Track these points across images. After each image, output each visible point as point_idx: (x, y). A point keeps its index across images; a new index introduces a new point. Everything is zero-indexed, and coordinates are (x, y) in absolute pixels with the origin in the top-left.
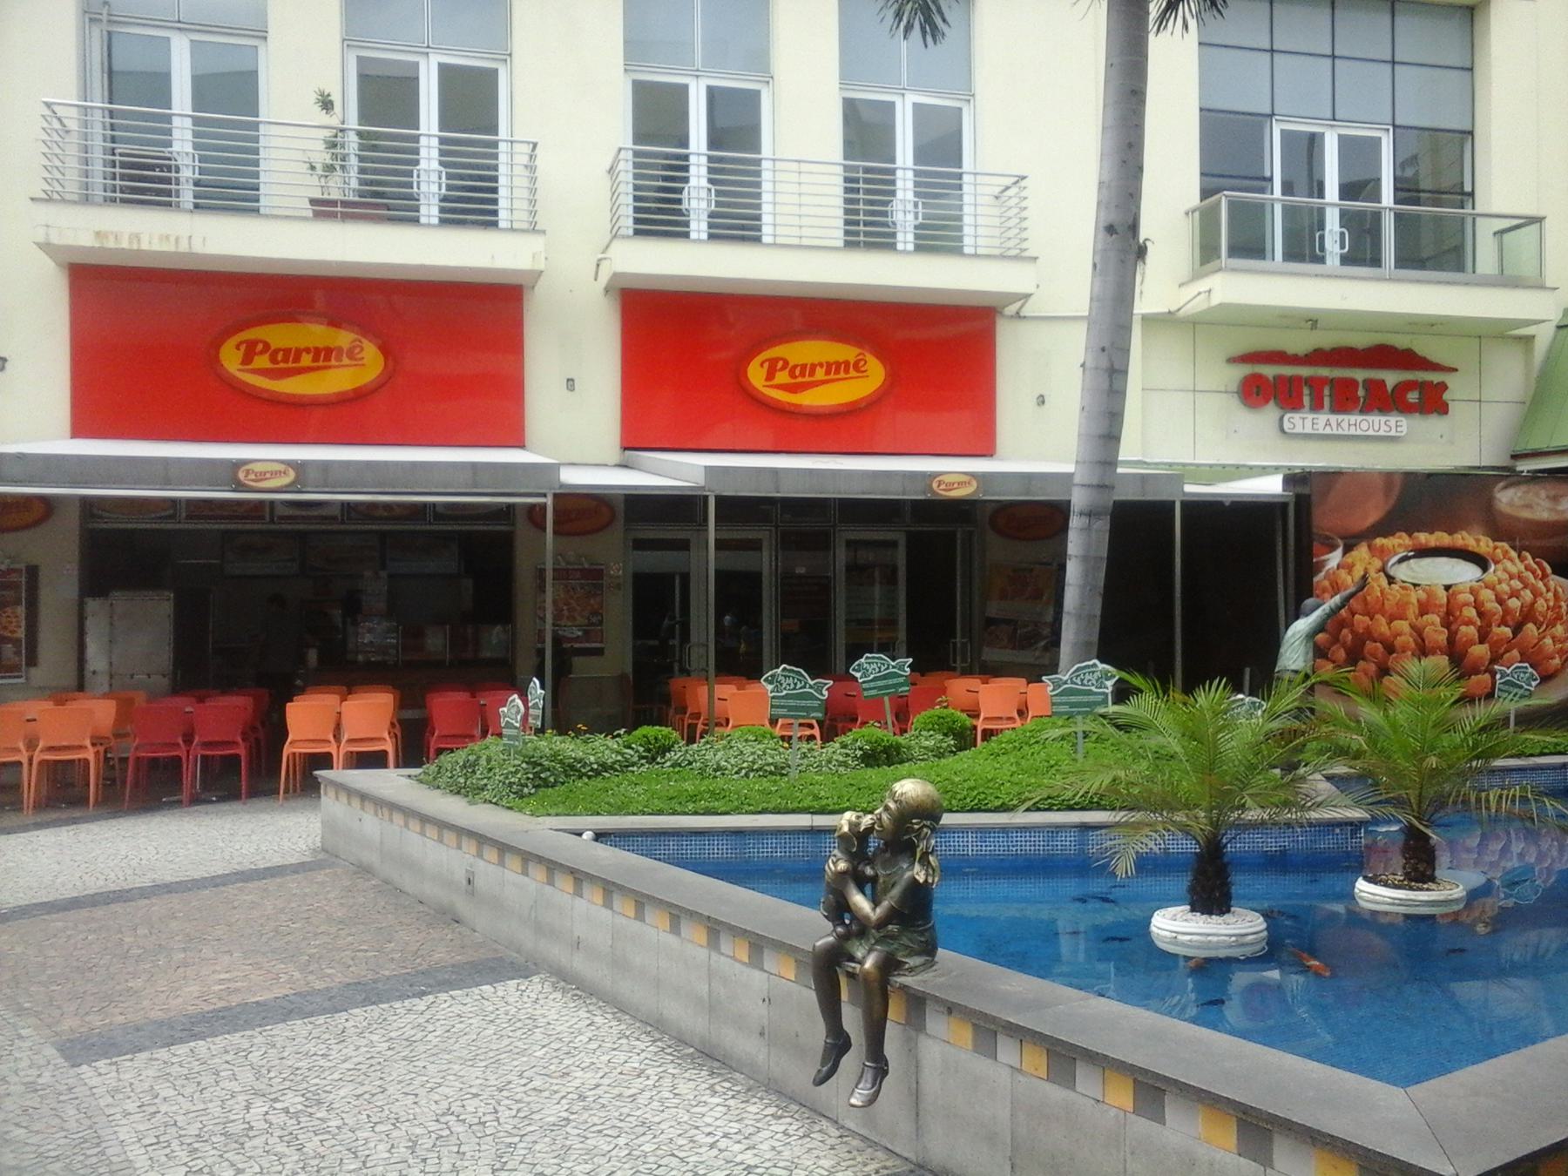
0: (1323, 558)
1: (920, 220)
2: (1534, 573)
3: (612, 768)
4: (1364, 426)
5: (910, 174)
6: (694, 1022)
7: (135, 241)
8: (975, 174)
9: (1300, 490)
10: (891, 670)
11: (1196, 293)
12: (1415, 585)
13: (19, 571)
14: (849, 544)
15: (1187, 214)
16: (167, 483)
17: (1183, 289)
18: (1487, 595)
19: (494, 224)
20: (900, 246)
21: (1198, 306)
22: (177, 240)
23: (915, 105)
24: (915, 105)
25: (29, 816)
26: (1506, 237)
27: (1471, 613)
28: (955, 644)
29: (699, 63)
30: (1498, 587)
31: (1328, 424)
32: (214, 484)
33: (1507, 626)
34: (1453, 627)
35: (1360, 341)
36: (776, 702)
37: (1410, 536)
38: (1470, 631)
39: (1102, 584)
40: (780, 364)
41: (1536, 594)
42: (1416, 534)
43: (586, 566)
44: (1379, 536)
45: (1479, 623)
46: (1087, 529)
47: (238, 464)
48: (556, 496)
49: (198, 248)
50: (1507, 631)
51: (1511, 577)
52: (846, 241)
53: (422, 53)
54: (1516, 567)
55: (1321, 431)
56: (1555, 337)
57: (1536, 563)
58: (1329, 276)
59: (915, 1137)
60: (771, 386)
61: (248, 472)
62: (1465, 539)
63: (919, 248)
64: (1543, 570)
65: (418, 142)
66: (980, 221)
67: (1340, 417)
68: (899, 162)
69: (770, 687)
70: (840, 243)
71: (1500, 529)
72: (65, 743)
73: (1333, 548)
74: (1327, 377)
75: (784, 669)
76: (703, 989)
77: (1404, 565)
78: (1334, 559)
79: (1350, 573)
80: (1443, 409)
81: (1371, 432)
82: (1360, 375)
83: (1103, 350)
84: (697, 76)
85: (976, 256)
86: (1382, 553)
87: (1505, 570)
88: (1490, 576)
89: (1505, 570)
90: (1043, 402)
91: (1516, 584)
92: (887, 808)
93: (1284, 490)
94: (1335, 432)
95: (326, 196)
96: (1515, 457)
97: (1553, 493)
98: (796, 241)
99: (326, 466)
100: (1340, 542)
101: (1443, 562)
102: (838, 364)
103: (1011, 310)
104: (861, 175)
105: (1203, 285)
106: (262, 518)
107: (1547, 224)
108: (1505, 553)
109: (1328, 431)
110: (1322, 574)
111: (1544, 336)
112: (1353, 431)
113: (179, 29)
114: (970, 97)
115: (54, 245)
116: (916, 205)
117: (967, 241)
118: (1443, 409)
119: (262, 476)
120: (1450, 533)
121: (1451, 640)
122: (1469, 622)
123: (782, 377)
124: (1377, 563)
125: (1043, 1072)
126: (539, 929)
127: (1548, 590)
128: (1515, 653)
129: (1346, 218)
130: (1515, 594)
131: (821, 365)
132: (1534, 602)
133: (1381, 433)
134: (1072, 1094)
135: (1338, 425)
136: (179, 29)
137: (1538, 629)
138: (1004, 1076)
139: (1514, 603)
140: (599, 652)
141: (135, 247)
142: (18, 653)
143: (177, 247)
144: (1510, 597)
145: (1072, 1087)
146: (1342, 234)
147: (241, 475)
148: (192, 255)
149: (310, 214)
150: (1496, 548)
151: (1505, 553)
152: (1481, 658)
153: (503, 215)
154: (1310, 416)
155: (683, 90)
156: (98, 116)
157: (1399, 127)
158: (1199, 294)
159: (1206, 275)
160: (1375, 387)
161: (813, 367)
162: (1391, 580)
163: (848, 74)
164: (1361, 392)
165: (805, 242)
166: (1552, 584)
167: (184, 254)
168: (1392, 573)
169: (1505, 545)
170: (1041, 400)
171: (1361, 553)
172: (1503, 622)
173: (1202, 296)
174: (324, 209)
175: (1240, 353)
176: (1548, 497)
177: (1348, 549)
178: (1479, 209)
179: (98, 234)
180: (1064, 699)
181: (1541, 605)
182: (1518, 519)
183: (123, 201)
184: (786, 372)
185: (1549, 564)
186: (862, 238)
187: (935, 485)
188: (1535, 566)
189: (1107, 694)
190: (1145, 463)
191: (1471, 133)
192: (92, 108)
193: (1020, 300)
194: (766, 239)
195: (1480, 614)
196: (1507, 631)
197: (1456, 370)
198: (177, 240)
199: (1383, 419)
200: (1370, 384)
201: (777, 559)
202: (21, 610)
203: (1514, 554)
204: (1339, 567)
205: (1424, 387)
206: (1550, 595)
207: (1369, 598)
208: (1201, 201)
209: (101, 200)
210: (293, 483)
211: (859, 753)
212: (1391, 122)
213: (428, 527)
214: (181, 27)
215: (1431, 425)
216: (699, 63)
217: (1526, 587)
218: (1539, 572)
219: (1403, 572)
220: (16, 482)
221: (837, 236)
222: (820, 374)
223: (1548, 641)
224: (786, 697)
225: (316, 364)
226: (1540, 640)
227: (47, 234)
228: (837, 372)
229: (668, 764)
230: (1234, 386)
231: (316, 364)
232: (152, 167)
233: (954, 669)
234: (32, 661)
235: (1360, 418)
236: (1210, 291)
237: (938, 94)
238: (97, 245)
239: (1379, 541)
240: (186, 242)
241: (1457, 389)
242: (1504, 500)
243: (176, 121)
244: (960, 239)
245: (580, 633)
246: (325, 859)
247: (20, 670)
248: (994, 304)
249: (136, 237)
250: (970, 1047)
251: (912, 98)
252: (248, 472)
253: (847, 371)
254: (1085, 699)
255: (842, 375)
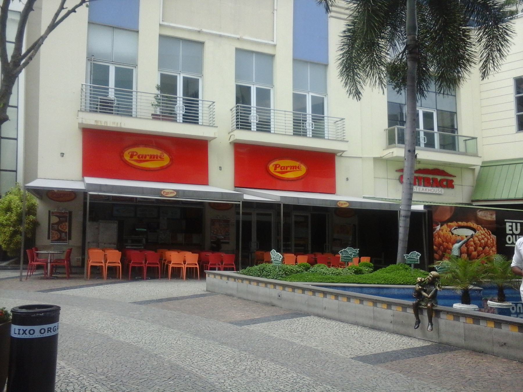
0: (436, 227)
1: (313, 128)
2: (487, 233)
3: (299, 272)
4: (433, 190)
5: (311, 116)
6: (371, 322)
7: (106, 123)
8: (328, 117)
9: (429, 209)
10: (354, 252)
11: (389, 152)
12: (458, 235)
13: (67, 213)
14: (295, 216)
15: (385, 130)
16: (143, 194)
17: (384, 151)
18: (476, 239)
19: (198, 123)
20: (308, 136)
21: (390, 156)
22: (117, 124)
23: (312, 96)
24: (312, 96)
25: (105, 281)
26: (468, 142)
27: (472, 243)
28: (326, 245)
29: (254, 81)
30: (479, 237)
31: (423, 189)
32: (155, 195)
33: (481, 247)
34: (468, 247)
35: (430, 167)
36: (342, 258)
37: (457, 222)
38: (472, 248)
39: (408, 233)
40: (278, 166)
41: (488, 239)
42: (458, 222)
43: (225, 219)
44: (449, 222)
45: (474, 246)
46: (405, 221)
47: (161, 190)
48: (242, 202)
49: (123, 126)
50: (481, 248)
51: (482, 234)
52: (294, 133)
53: (178, 73)
54: (483, 232)
55: (421, 192)
56: (480, 169)
57: (488, 231)
58: (421, 150)
59: (438, 337)
60: (276, 172)
61: (164, 192)
62: (470, 224)
63: (313, 137)
64: (489, 233)
65: (177, 99)
66: (329, 130)
67: (426, 188)
68: (308, 112)
69: (341, 254)
70: (292, 134)
71: (479, 222)
72: (114, 261)
73: (438, 225)
74: (422, 177)
75: (344, 250)
76: (372, 315)
77: (455, 230)
78: (438, 228)
79: (442, 232)
80: (452, 187)
81: (434, 192)
82: (431, 176)
83: (408, 179)
84: (253, 84)
85: (328, 139)
86: (450, 227)
87: (480, 232)
88: (477, 234)
89: (480, 232)
90: (348, 180)
91: (483, 236)
92: (430, 277)
93: (424, 209)
94: (425, 192)
95: (156, 113)
96: (473, 201)
97: (491, 213)
98: (284, 133)
99: (184, 191)
100: (440, 223)
101: (465, 230)
102: (294, 167)
103: (339, 154)
104: (301, 116)
105: (391, 150)
106: (134, 201)
107: (478, 139)
108: (480, 228)
109: (423, 191)
110: (435, 232)
111: (477, 169)
112: (429, 192)
113: (112, 63)
114: (326, 95)
115: (84, 124)
116: (312, 124)
117: (326, 135)
118: (452, 187)
119: (168, 193)
120: (467, 223)
121: (468, 250)
122: (472, 246)
123: (279, 170)
124: (449, 229)
125: (472, 322)
126: (309, 305)
127: (491, 238)
128: (483, 254)
129: (425, 134)
130: (483, 239)
131: (289, 167)
132: (488, 241)
133: (437, 193)
134: (480, 326)
135: (426, 190)
136: (112, 63)
137: (489, 248)
138: (462, 324)
139: (483, 241)
140: (228, 243)
141: (106, 125)
142: (66, 236)
143: (415, 192)
144: (482, 239)
145: (480, 325)
146: (425, 138)
147: (162, 193)
148: (121, 128)
149: (151, 118)
150: (478, 227)
151: (480, 228)
152: (475, 255)
153: (200, 121)
154: (418, 187)
155: (249, 88)
156: (89, 88)
157: (438, 110)
158: (390, 153)
159: (391, 148)
160: (435, 180)
161: (287, 167)
162: (452, 234)
163: (295, 87)
164: (431, 181)
165: (287, 133)
166: (492, 237)
167: (119, 128)
168: (453, 232)
169: (480, 226)
170: (347, 179)
171: (445, 226)
172: (480, 246)
173: (391, 153)
174: (155, 117)
175: (399, 169)
176: (490, 214)
177: (441, 226)
178: (459, 134)
179: (96, 121)
180: (409, 260)
181: (489, 242)
182: (483, 219)
183: (100, 112)
184: (279, 168)
185: (491, 231)
186: (302, 133)
187: (338, 204)
188: (487, 232)
189: (418, 259)
190: (375, 198)
191: (456, 113)
192: (87, 85)
193: (340, 152)
194: (272, 132)
195: (475, 244)
196: (481, 248)
197: (456, 177)
198: (117, 124)
199: (438, 189)
200: (433, 179)
201: (276, 219)
202: (67, 224)
203: (482, 229)
204: (440, 230)
205: (447, 181)
206: (491, 239)
207: (447, 238)
208: (388, 127)
209: (88, 111)
210: (176, 195)
211: (354, 271)
212: (435, 108)
213: (180, 206)
214: (113, 63)
215: (449, 191)
216: (254, 81)
217: (485, 237)
218: (488, 233)
219: (455, 232)
220: (104, 192)
221: (291, 132)
222: (289, 169)
223: (491, 251)
224: (344, 257)
225: (150, 159)
226: (489, 251)
227: (82, 121)
228: (293, 169)
229: (311, 271)
230: (398, 178)
231: (150, 159)
232: (108, 103)
233: (326, 252)
234: (70, 238)
235: (431, 188)
236: (393, 152)
237: (316, 93)
238: (96, 124)
239: (449, 224)
240: (120, 124)
241: (456, 182)
242: (479, 214)
243: (110, 90)
244: (324, 134)
245: (223, 238)
246: (211, 292)
247: (67, 240)
248: (334, 152)
249: (106, 122)
250: (453, 319)
251: (311, 94)
252: (164, 192)
253: (296, 169)
254: (413, 260)
255: (295, 170)
